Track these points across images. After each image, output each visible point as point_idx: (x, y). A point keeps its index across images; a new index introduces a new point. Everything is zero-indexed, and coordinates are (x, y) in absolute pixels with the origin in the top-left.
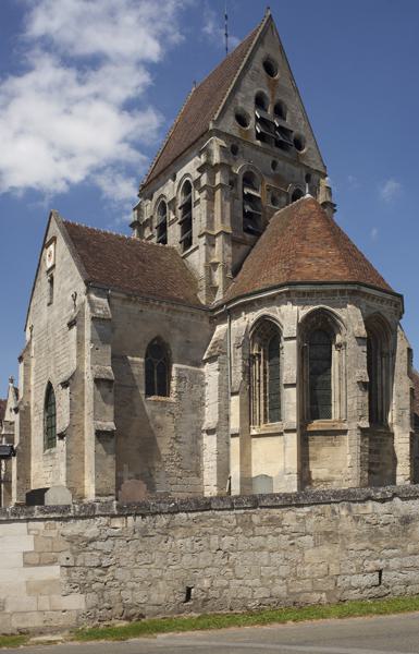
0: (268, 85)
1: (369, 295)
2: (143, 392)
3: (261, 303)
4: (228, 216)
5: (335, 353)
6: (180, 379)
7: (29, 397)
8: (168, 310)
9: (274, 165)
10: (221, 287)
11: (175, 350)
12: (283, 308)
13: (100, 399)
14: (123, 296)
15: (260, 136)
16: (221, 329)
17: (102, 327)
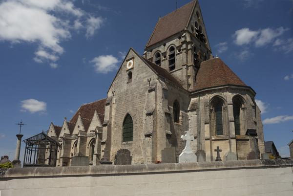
3: (215, 91)
4: (193, 60)
5: (241, 111)
6: (183, 116)
7: (111, 120)
10: (192, 84)
12: (225, 93)
14: (168, 82)
16: (193, 100)
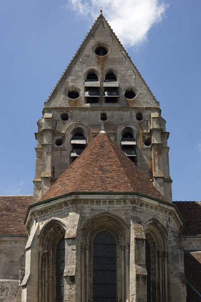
1: (92, 201)
9: (104, 117)
15: (88, 100)
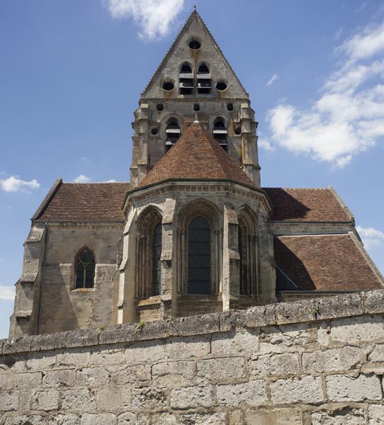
0: (192, 56)
1: (188, 187)
2: (68, 287)
6: (100, 275)
8: (93, 227)
9: (197, 108)
11: (97, 254)
13: (24, 295)
14: (58, 224)
17: (34, 247)
